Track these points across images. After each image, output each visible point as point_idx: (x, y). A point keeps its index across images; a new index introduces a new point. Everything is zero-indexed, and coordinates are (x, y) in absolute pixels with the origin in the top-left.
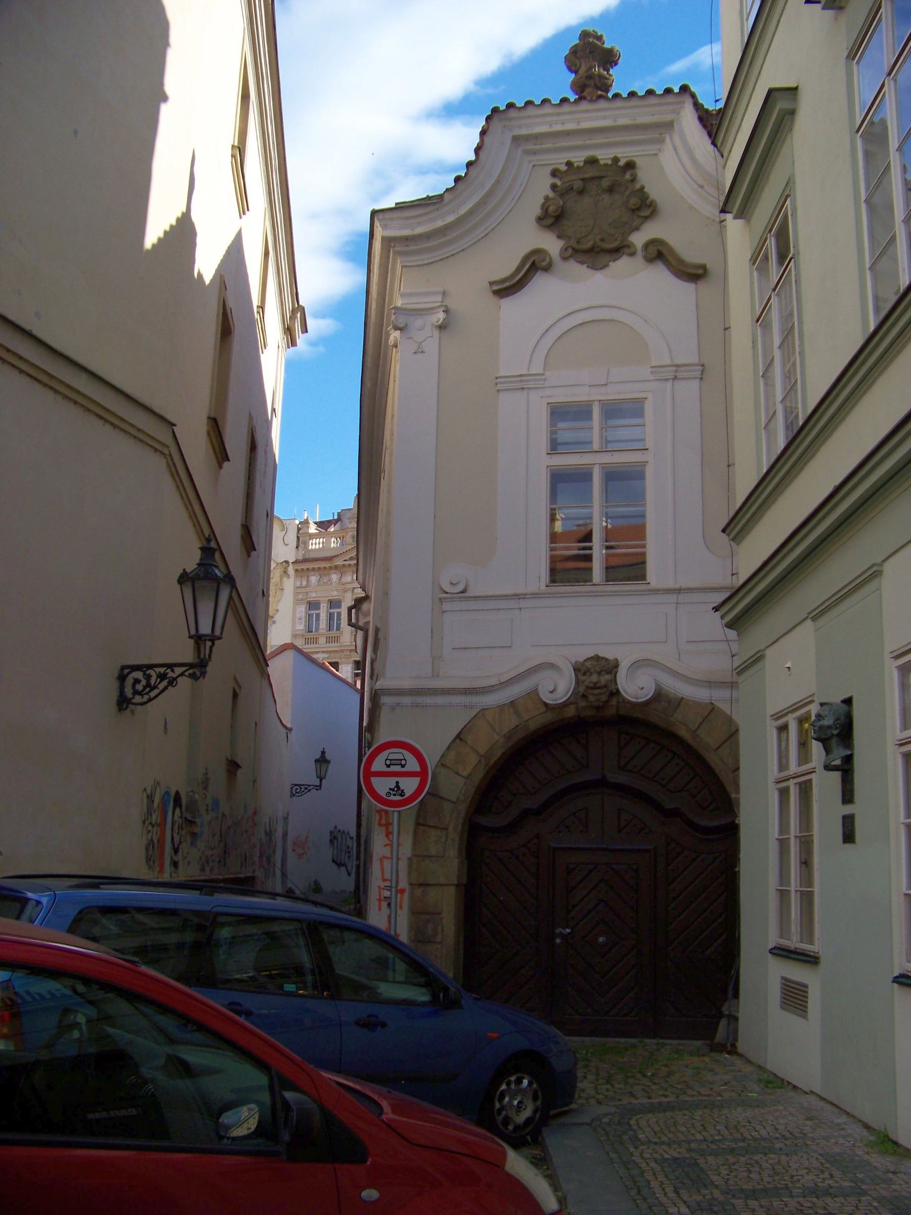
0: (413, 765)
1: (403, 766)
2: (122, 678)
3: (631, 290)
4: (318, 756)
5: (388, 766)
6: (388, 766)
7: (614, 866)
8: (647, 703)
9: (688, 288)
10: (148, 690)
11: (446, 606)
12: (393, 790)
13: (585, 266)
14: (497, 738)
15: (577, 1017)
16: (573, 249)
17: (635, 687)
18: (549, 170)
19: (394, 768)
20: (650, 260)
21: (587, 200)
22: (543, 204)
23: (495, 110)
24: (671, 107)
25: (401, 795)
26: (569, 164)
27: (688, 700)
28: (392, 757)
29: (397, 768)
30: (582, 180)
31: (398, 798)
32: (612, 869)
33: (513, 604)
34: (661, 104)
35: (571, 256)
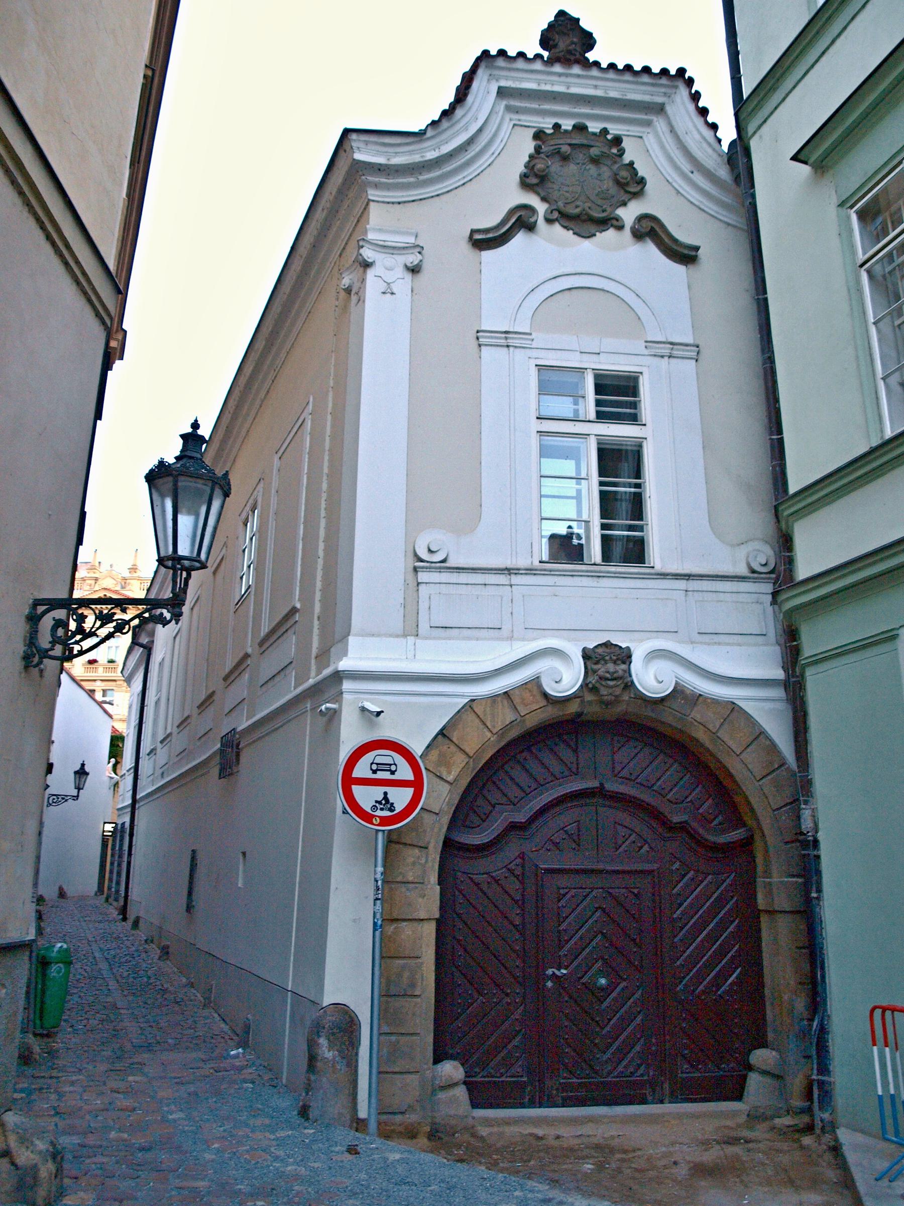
0: (405, 772)
1: (393, 773)
2: (33, 619)
4: (78, 767)
5: (374, 772)
6: (374, 772)
7: (610, 890)
8: (663, 700)
9: (679, 269)
10: (78, 637)
11: (423, 576)
12: (380, 802)
13: (571, 232)
14: (489, 735)
15: (574, 1080)
16: (560, 212)
17: (651, 678)
18: (533, 131)
19: (381, 775)
20: (638, 235)
21: (572, 168)
23: (486, 53)
24: (663, 90)
25: (391, 810)
26: (557, 126)
27: (707, 698)
28: (379, 760)
29: (385, 775)
30: (570, 145)
31: (386, 813)
32: (471, 879)
33: (502, 579)
34: (653, 85)
35: (557, 220)
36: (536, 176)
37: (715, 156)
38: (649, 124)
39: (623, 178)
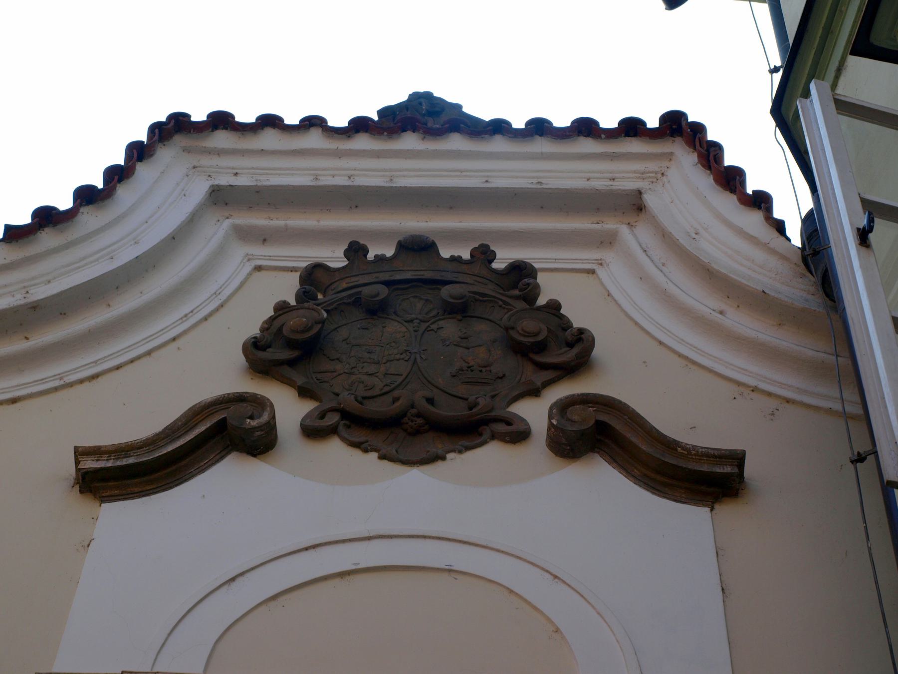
3: (516, 510)
9: (690, 520)
13: (374, 456)
16: (345, 414)
21: (393, 328)
22: (272, 320)
30: (387, 283)
36: (291, 344)
37: (773, 262)
38: (608, 241)
39: (528, 334)
